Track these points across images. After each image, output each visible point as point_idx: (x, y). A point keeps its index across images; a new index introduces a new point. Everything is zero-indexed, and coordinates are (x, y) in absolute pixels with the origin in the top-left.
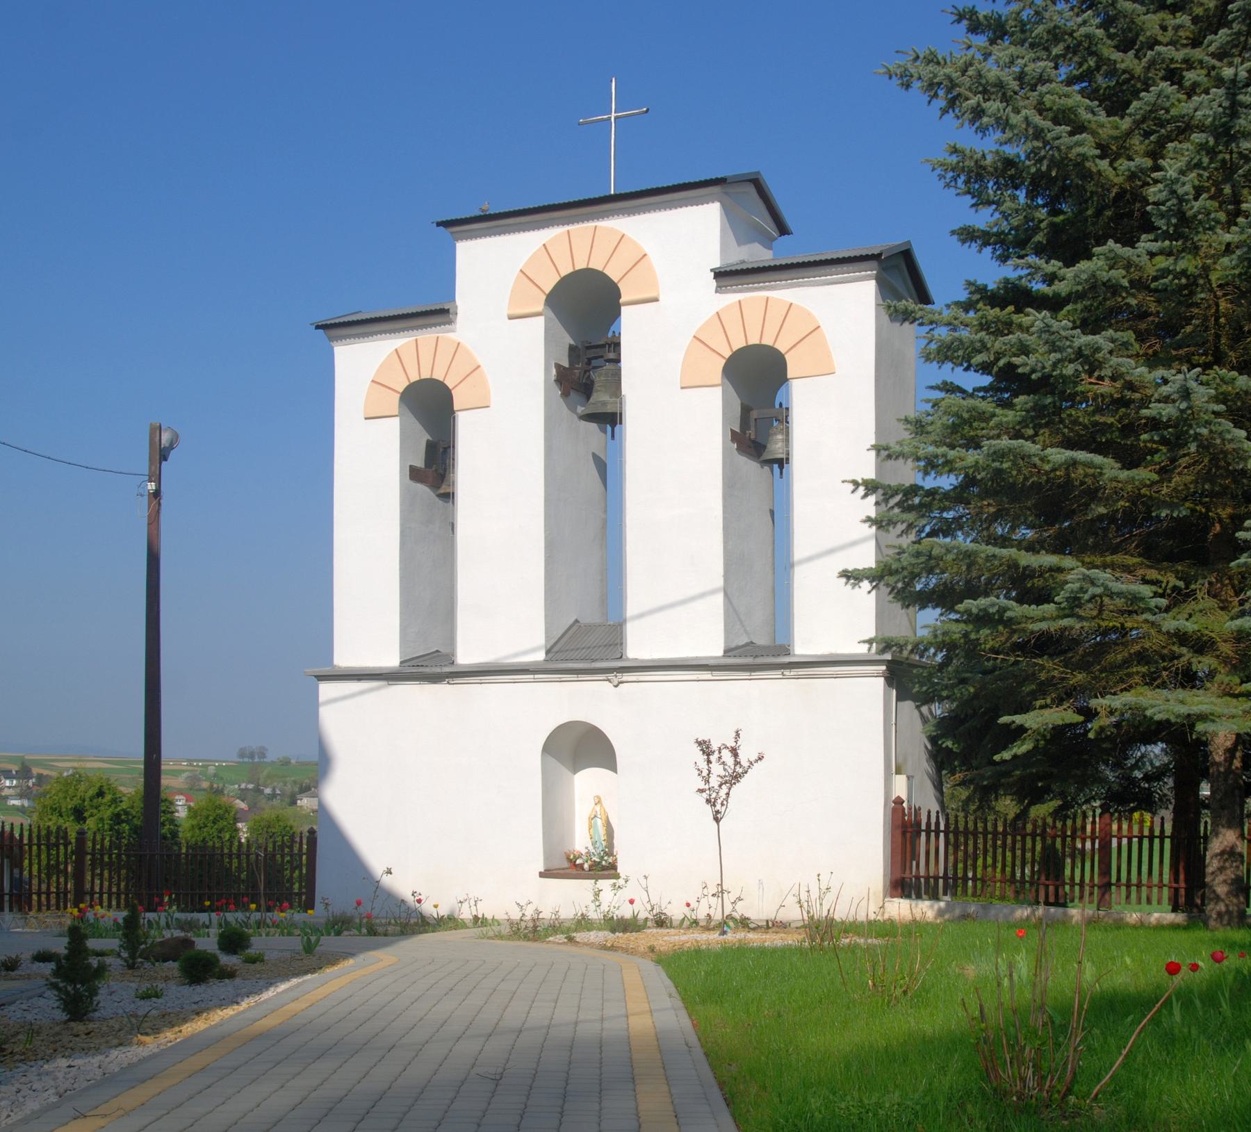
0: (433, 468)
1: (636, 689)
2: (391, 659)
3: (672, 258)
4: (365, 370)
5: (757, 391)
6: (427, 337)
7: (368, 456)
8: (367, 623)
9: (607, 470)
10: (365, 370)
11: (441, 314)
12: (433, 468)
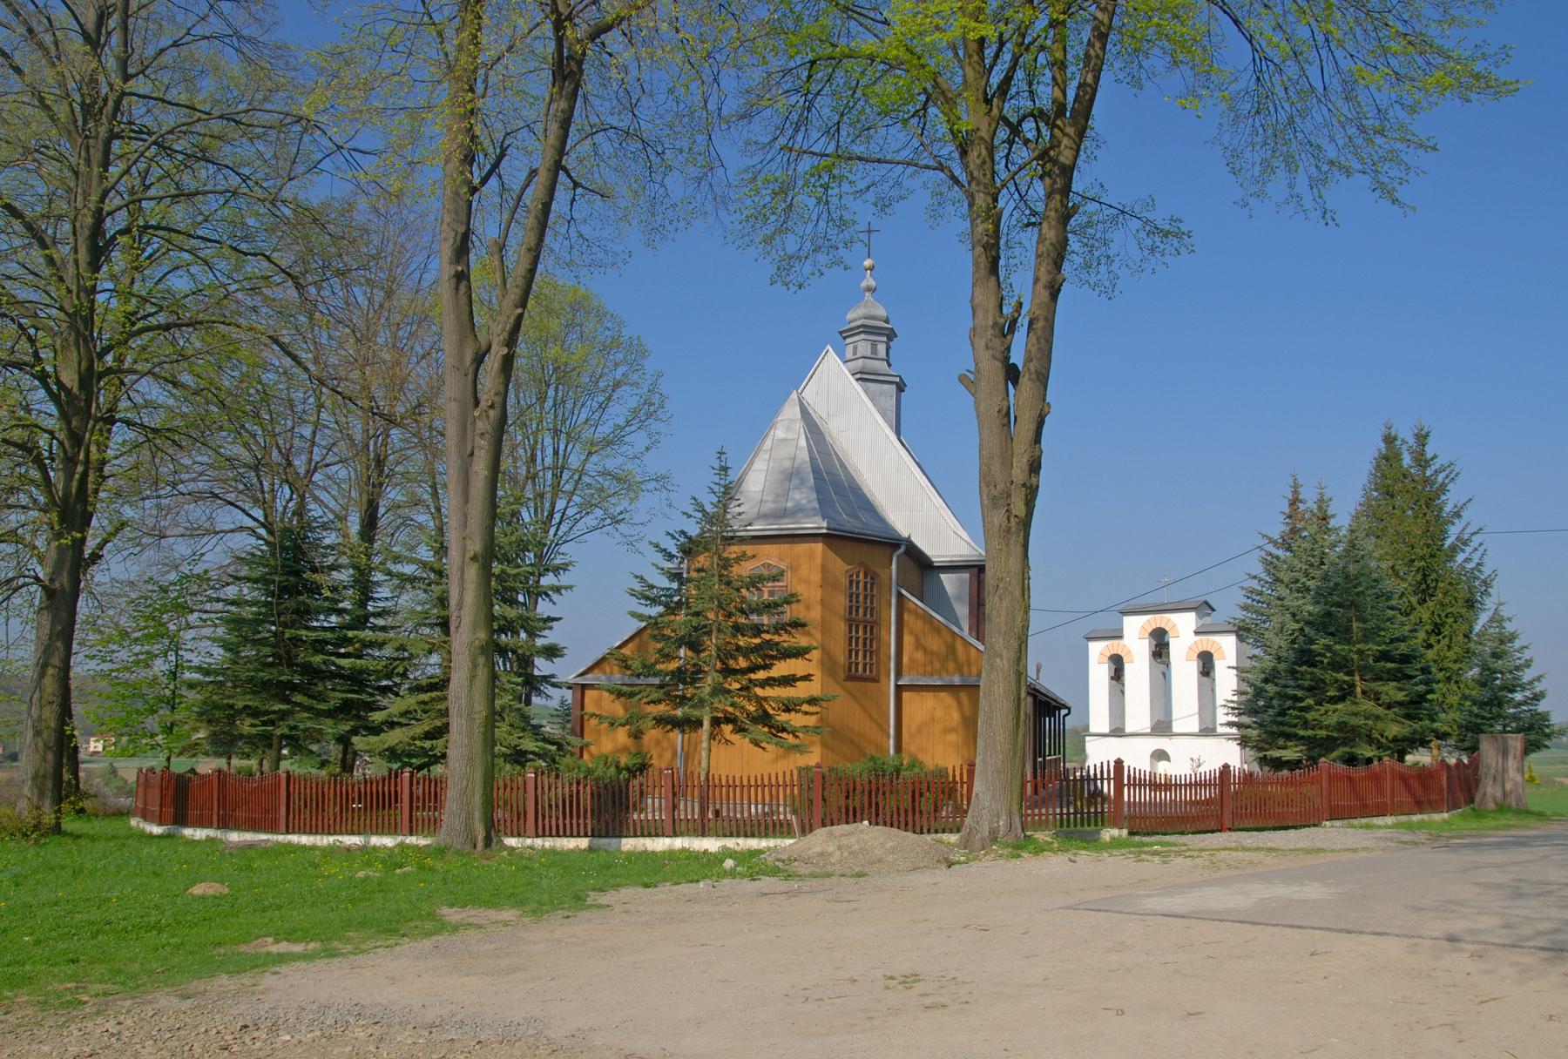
0: (1118, 674)
1: (1175, 740)
2: (1107, 731)
3: (1183, 626)
4: (1098, 651)
5: (1206, 663)
6: (1116, 642)
7: (1099, 674)
8: (1099, 720)
9: (1166, 676)
10: (1098, 651)
11: (1121, 637)
12: (1118, 674)
